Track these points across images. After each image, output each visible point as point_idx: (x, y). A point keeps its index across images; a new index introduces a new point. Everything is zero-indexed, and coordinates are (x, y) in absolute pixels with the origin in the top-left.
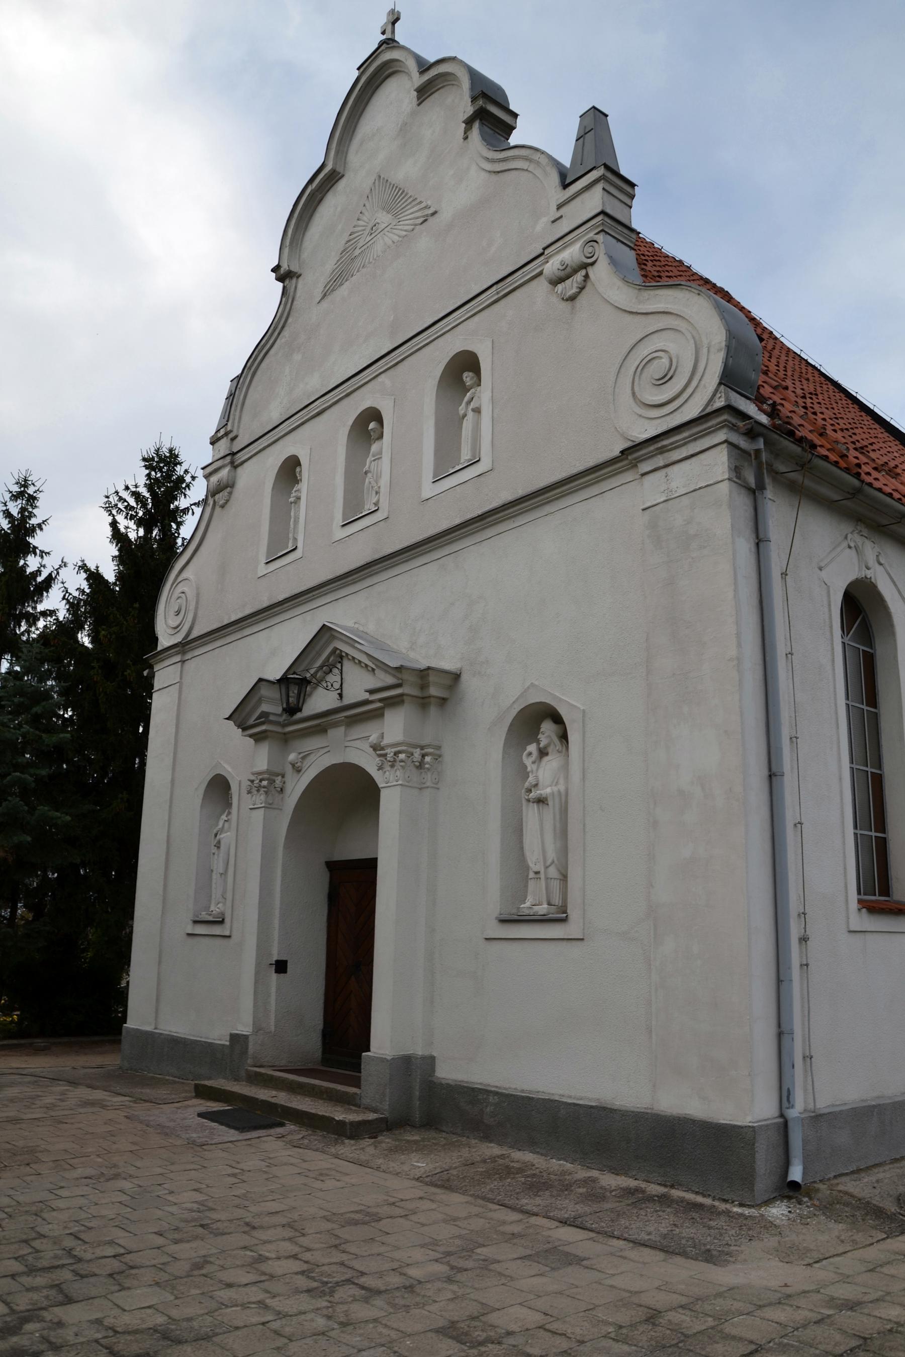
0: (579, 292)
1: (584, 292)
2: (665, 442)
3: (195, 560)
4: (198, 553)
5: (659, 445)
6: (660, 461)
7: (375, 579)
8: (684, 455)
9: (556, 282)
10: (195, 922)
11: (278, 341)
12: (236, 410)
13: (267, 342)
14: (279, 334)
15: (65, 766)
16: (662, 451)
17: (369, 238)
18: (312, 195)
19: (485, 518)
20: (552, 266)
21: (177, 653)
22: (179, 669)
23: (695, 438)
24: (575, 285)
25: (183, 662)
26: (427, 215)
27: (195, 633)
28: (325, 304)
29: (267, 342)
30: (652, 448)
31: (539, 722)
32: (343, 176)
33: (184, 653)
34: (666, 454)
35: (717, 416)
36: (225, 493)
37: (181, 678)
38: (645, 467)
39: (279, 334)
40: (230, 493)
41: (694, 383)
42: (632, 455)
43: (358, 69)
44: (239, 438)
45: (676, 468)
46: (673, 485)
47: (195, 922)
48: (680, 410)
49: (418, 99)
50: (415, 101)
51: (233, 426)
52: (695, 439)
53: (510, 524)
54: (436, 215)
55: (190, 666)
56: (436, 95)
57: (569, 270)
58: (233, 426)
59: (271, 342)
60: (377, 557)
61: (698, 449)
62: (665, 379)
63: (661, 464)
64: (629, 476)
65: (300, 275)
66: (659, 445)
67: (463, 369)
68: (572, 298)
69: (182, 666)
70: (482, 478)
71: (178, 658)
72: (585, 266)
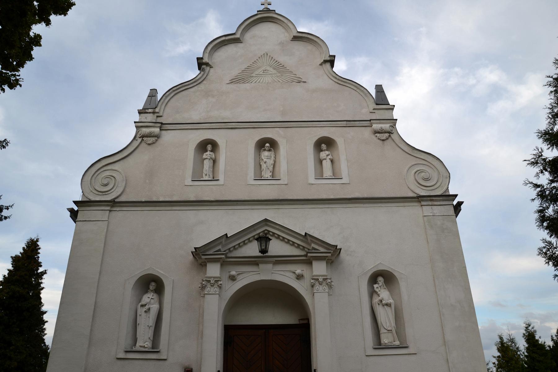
3: (121, 162)
4: (125, 160)
6: (430, 203)
7: (281, 207)
9: (376, 132)
10: (126, 352)
11: (196, 87)
13: (189, 85)
15: (36, 3)
18: (224, 41)
21: (108, 206)
23: (443, 200)
25: (110, 211)
27: (123, 199)
28: (232, 86)
29: (189, 85)
31: (383, 277)
33: (112, 206)
36: (153, 139)
38: (423, 203)
40: (157, 140)
41: (107, 193)
42: (419, 199)
45: (435, 207)
46: (435, 212)
47: (126, 352)
51: (160, 110)
53: (362, 205)
55: (113, 213)
58: (160, 110)
59: (189, 87)
64: (416, 204)
71: (109, 208)
72: (389, 133)
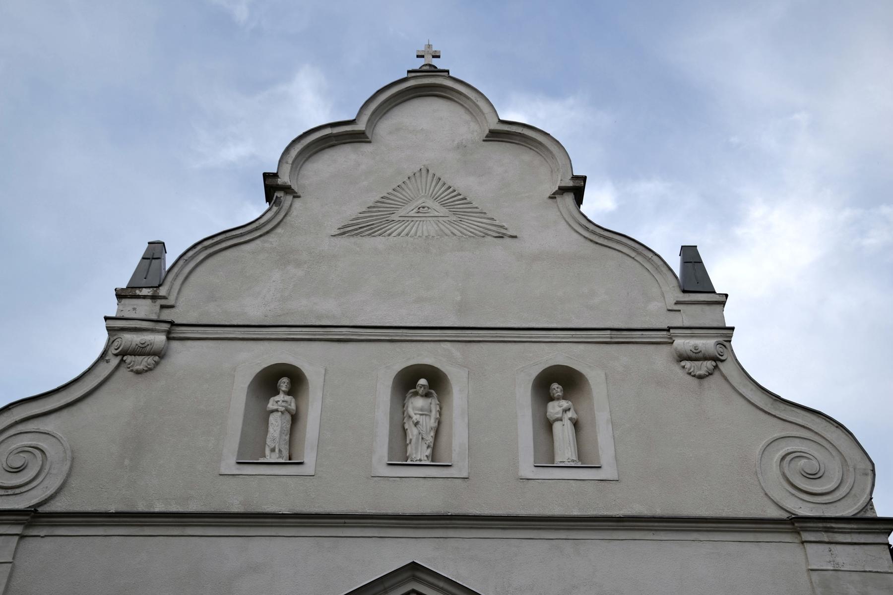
0: (146, 371)
1: (711, 377)
2: (834, 525)
5: (829, 525)
6: (825, 537)
8: (849, 540)
9: (682, 357)
12: (175, 279)
13: (242, 235)
14: (261, 236)
16: (827, 530)
17: (412, 214)
19: (623, 521)
20: (683, 343)
22: (15, 545)
23: (860, 532)
24: (144, 363)
25: (22, 537)
26: (504, 234)
27: (58, 506)
29: (242, 235)
30: (820, 525)
32: (370, 142)
33: (28, 525)
34: (830, 534)
35: (866, 524)
36: (150, 360)
37: (14, 558)
38: (806, 536)
39: (261, 236)
42: (795, 524)
43: (409, 72)
44: (172, 310)
48: (835, 504)
49: (487, 136)
50: (483, 137)
52: (860, 533)
53: (650, 535)
54: (515, 240)
55: (30, 544)
56: (508, 145)
57: (700, 355)
60: (452, 511)
61: (862, 541)
62: (813, 476)
63: (826, 540)
65: (299, 197)
66: (829, 525)
67: (558, 382)
68: (700, 377)
69: (18, 543)
70: (603, 483)
71: (18, 530)
72: (715, 359)
